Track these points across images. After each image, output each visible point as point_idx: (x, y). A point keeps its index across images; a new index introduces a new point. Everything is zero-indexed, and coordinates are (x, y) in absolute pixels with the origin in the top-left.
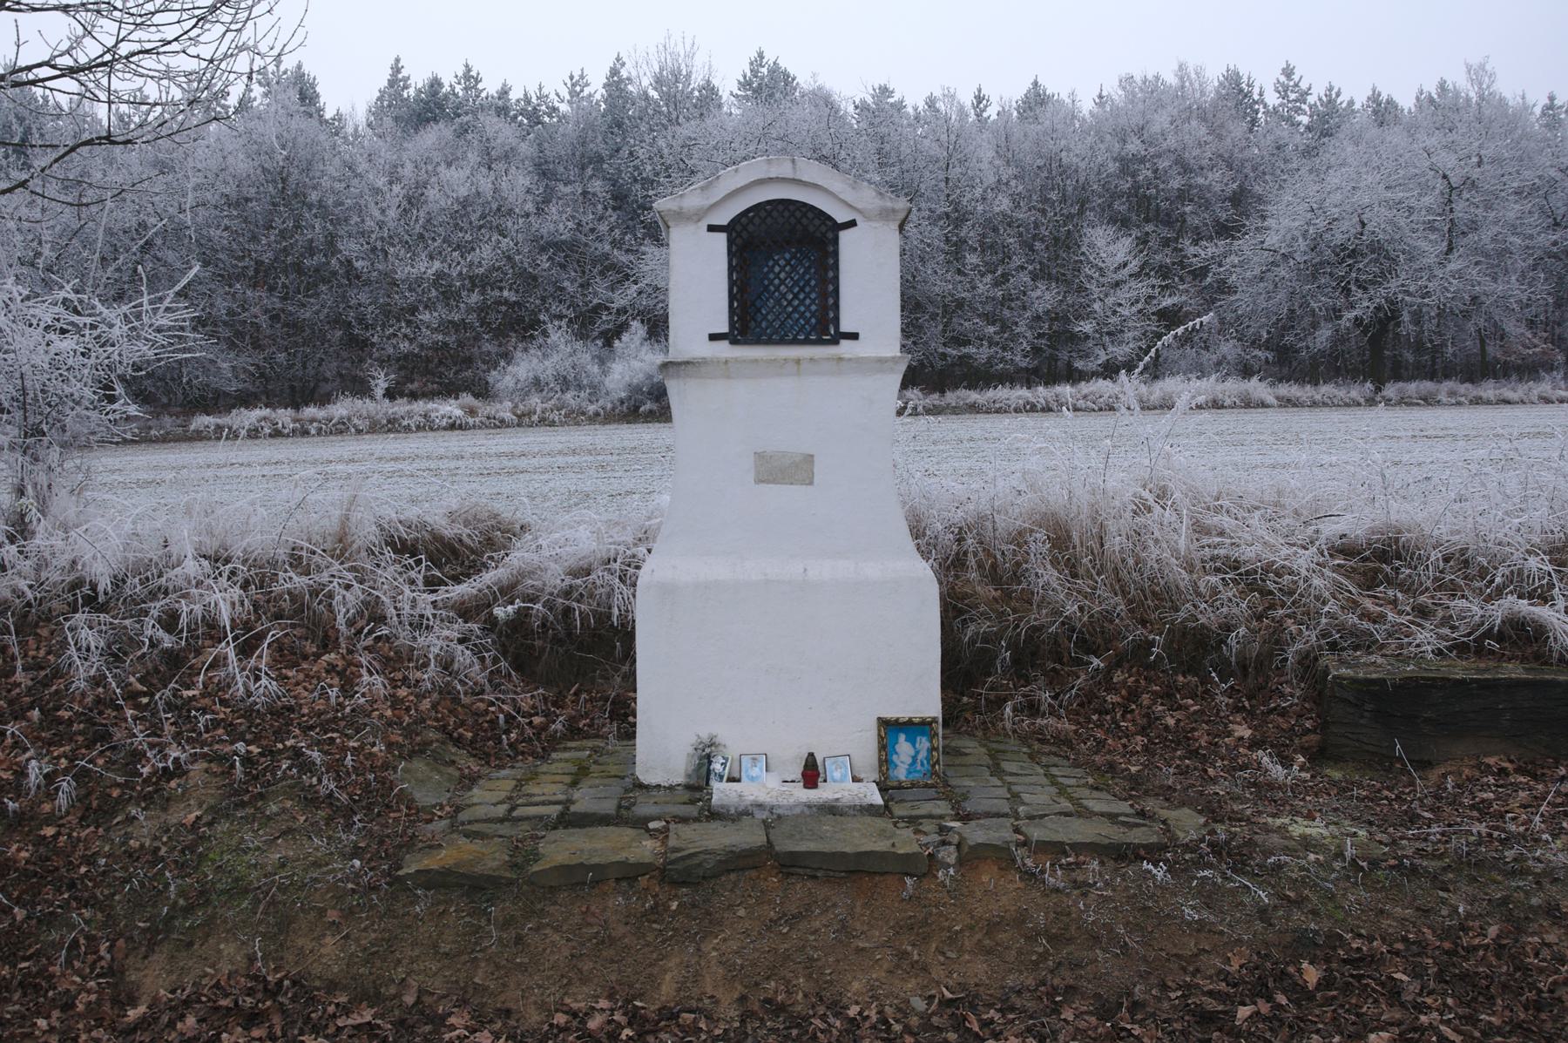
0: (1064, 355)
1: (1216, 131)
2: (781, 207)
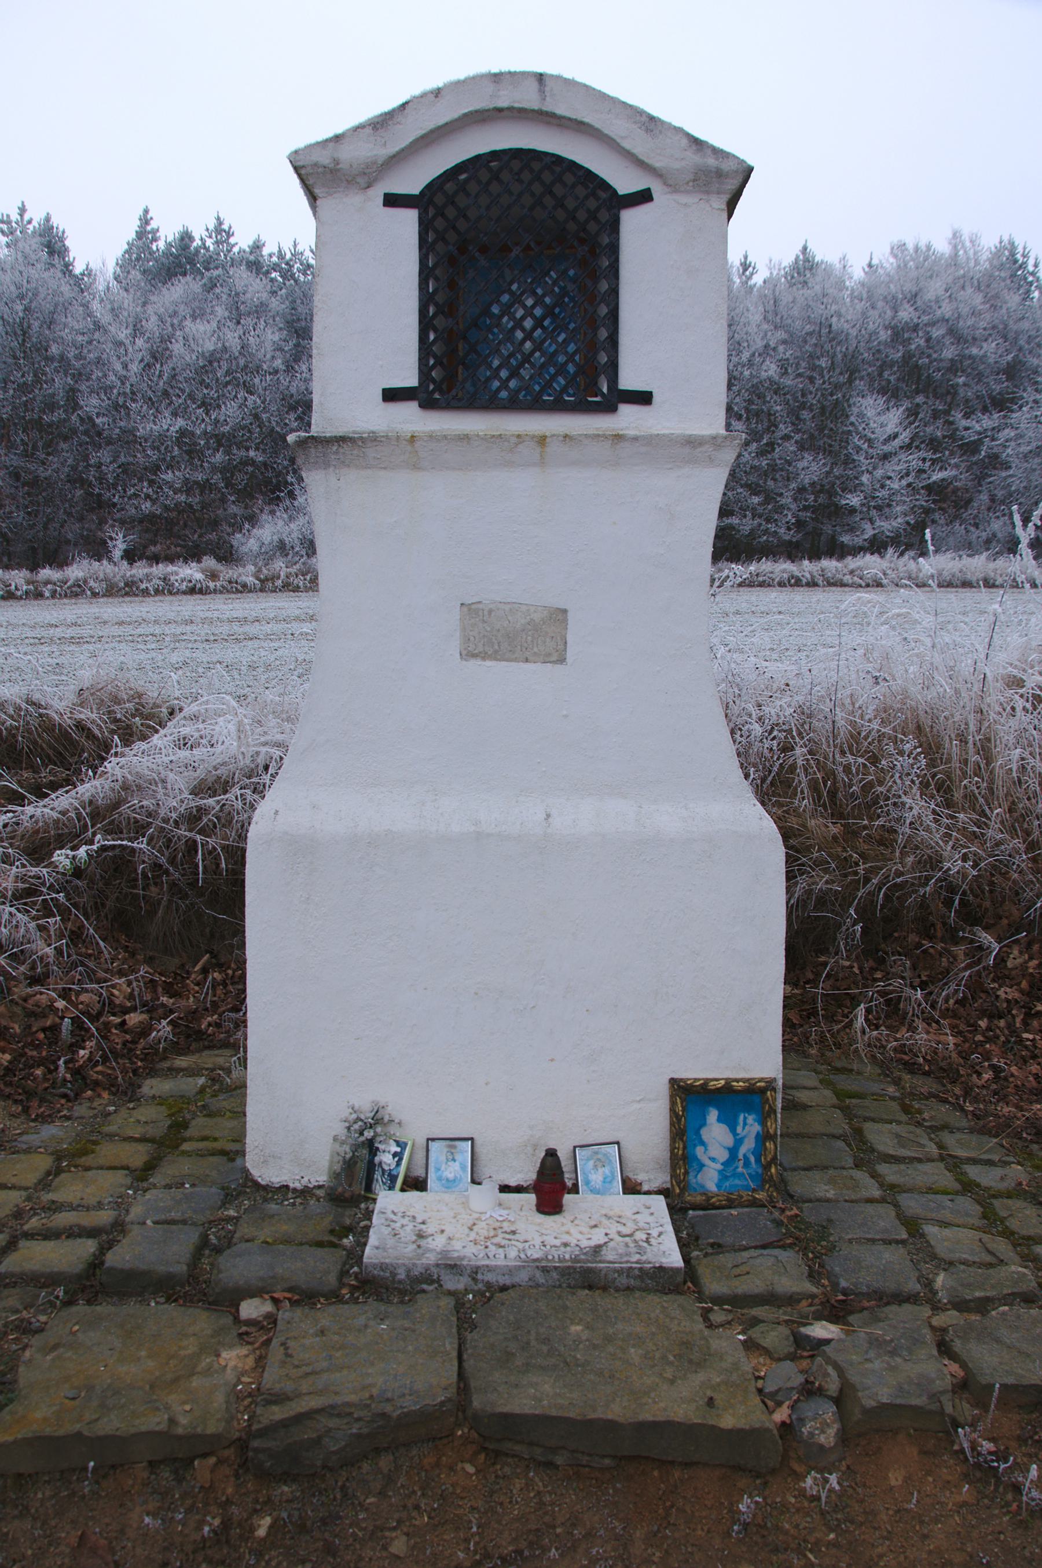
0: (828, 529)
1: (993, 302)
2: (516, 165)
